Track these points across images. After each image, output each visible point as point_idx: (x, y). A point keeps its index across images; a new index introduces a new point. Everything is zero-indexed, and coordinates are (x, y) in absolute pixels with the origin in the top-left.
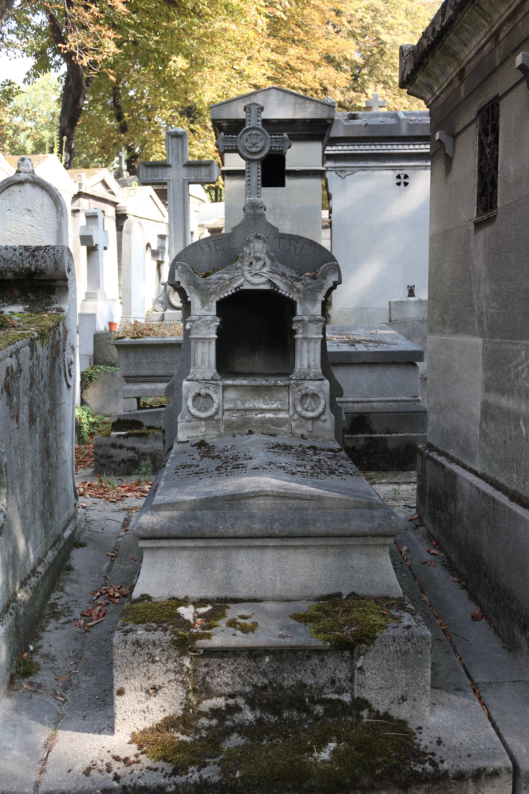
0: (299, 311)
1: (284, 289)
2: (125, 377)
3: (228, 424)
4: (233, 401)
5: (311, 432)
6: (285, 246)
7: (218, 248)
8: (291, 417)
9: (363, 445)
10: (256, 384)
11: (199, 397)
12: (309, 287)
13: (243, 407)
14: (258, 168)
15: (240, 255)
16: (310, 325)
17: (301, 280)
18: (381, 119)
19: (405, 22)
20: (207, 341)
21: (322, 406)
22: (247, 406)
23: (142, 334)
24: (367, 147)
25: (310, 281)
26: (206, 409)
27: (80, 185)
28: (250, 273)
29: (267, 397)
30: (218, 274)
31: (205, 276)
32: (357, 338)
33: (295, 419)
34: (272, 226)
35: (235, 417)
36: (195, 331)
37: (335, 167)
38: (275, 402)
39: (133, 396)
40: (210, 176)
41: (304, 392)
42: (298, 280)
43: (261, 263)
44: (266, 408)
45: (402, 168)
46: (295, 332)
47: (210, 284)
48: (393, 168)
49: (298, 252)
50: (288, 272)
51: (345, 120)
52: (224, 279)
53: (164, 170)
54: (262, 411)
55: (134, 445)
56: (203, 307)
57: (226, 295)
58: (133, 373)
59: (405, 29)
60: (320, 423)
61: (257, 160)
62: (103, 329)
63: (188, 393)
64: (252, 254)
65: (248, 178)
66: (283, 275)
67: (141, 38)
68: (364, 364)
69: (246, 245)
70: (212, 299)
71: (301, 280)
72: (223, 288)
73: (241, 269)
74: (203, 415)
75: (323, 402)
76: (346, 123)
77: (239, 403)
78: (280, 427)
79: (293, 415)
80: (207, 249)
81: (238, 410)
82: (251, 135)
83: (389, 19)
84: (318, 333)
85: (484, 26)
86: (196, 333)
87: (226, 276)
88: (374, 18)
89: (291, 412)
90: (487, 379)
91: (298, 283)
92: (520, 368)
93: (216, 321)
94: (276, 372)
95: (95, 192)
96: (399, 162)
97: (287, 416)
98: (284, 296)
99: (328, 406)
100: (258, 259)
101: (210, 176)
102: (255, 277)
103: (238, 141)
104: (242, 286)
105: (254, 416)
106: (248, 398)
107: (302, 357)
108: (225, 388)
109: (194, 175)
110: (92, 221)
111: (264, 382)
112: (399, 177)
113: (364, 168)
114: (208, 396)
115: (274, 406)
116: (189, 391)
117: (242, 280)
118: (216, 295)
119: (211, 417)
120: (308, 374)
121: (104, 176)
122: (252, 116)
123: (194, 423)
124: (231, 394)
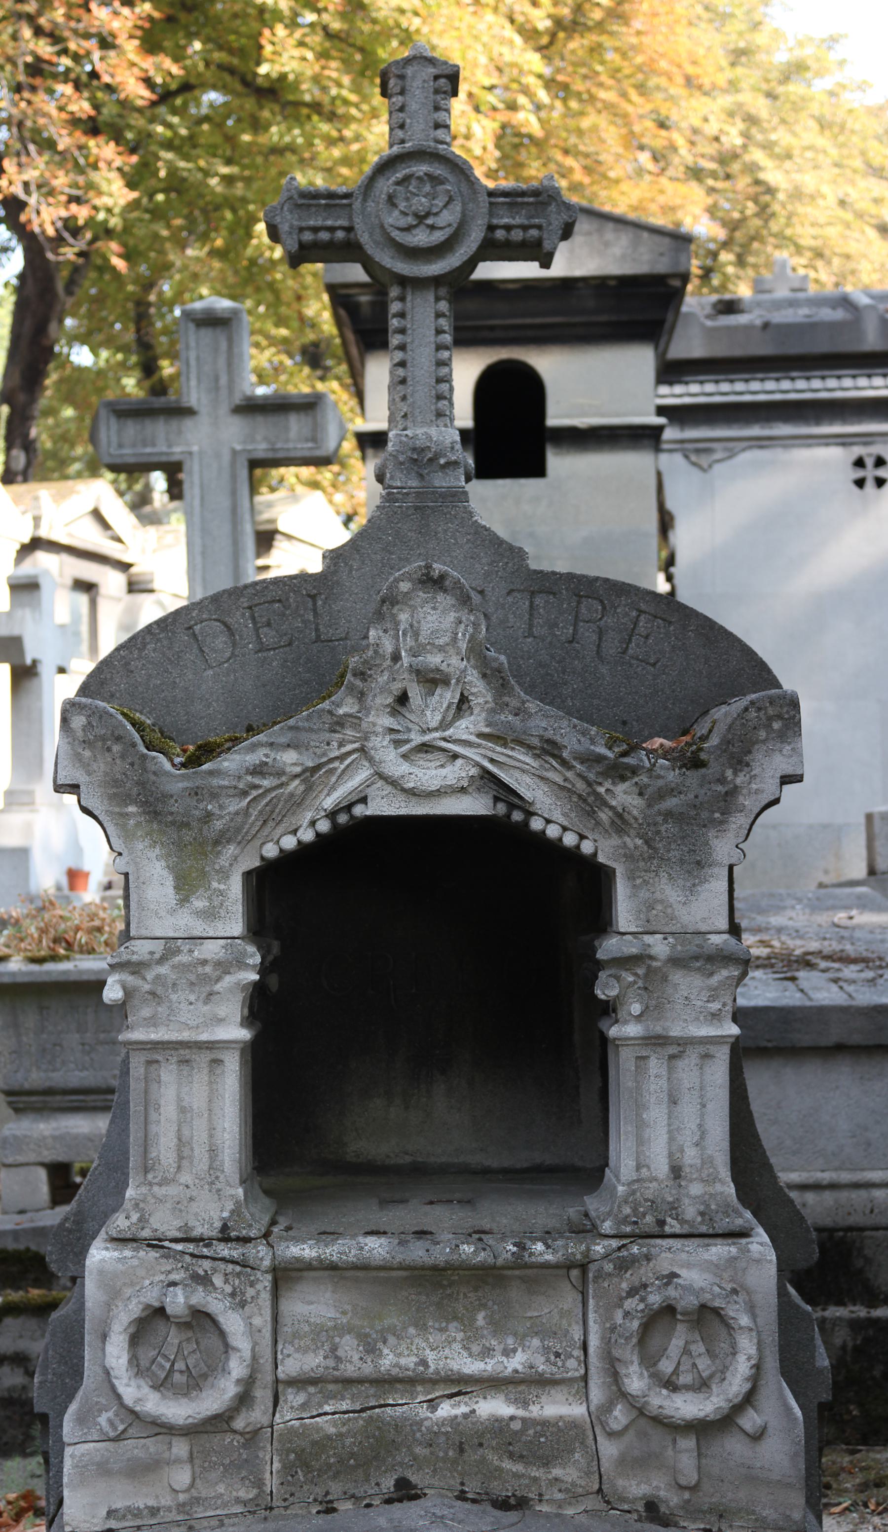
0: (625, 911)
1: (557, 816)
2: (9, 1093)
3: (300, 1454)
4: (323, 1336)
5: (694, 1489)
6: (553, 625)
7: (268, 636)
8: (598, 1418)
9: (844, 1347)
10: (429, 1261)
11: (161, 1326)
12: (671, 803)
13: (368, 1369)
14: (439, 315)
15: (354, 661)
16: (677, 977)
17: (635, 771)
18: (804, 311)
19: (822, 142)
20: (202, 1059)
21: (742, 1367)
22: (388, 1361)
23: (69, 946)
24: (770, 385)
25: (672, 776)
26: (194, 1384)
27: (37, 520)
28: (397, 743)
29: (481, 1319)
30: (253, 748)
31: (193, 761)
32: (799, 947)
33: (616, 1426)
34: (496, 542)
35: (331, 1417)
36: (146, 1012)
37: (682, 441)
38: (521, 1339)
39: (32, 1157)
40: (314, 439)
41: (655, 1299)
42: (619, 772)
43: (448, 696)
44: (477, 1374)
45: (867, 439)
46: (608, 1009)
47: (214, 796)
48: (844, 441)
49: (611, 647)
50: (571, 737)
51: (708, 317)
52: (280, 773)
53: (174, 423)
54: (461, 1385)
55: (23, 1345)
56: (184, 900)
57: (289, 843)
58: (36, 1078)
59: (821, 157)
60: (734, 1446)
61: (436, 281)
62: (52, 891)
63: (108, 1306)
64: (406, 659)
65: (399, 356)
66: (549, 749)
67: (189, 170)
68: (840, 1049)
69: (379, 616)
70: (223, 861)
71: (635, 771)
72: (275, 814)
73: (356, 727)
74: (178, 1411)
75: (747, 1346)
76: (709, 323)
77: (349, 1346)
78: (546, 1463)
79: (607, 1408)
80: (221, 641)
81: (348, 1382)
82: (406, 179)
83: (781, 137)
84: (715, 1016)
86: (153, 1022)
87: (289, 758)
88: (746, 135)
89: (597, 1394)
91: (620, 788)
93: (241, 964)
94: (522, 1159)
95: (70, 535)
96: (860, 422)
97: (578, 1410)
98: (556, 846)
99: (772, 1364)
100: (432, 680)
101: (314, 439)
102: (421, 761)
103: (357, 205)
104: (364, 800)
105: (423, 1412)
106: (392, 1320)
107: (640, 1125)
108: (284, 1276)
109: (266, 439)
110: (25, 597)
111: (467, 1249)
112: (859, 463)
113: (761, 442)
114: (201, 1319)
115: (516, 1363)
116: (113, 1294)
117: (363, 774)
118: (244, 843)
119: (219, 1422)
120: (674, 1208)
121: (98, 499)
122: (413, 106)
123: (137, 1448)
124: (312, 1306)
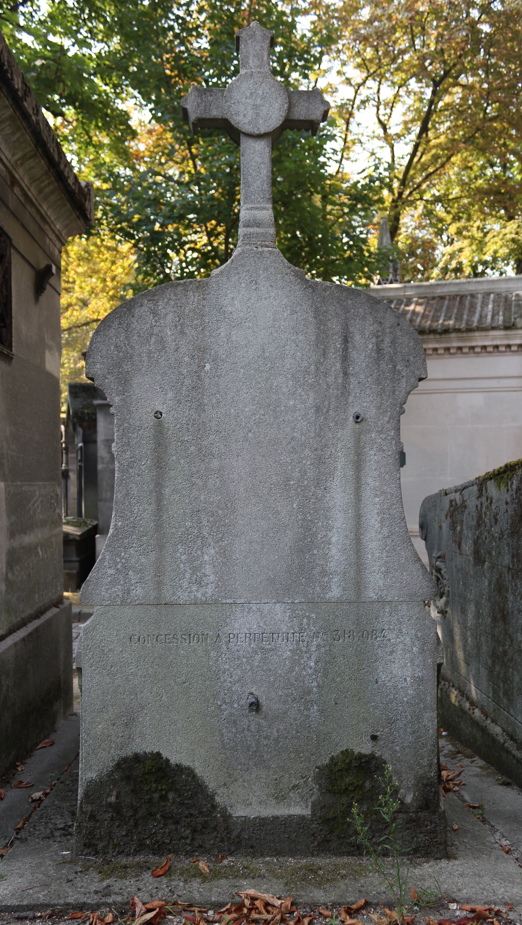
85: (13, 155)
90: (12, 524)
92: (36, 505)
